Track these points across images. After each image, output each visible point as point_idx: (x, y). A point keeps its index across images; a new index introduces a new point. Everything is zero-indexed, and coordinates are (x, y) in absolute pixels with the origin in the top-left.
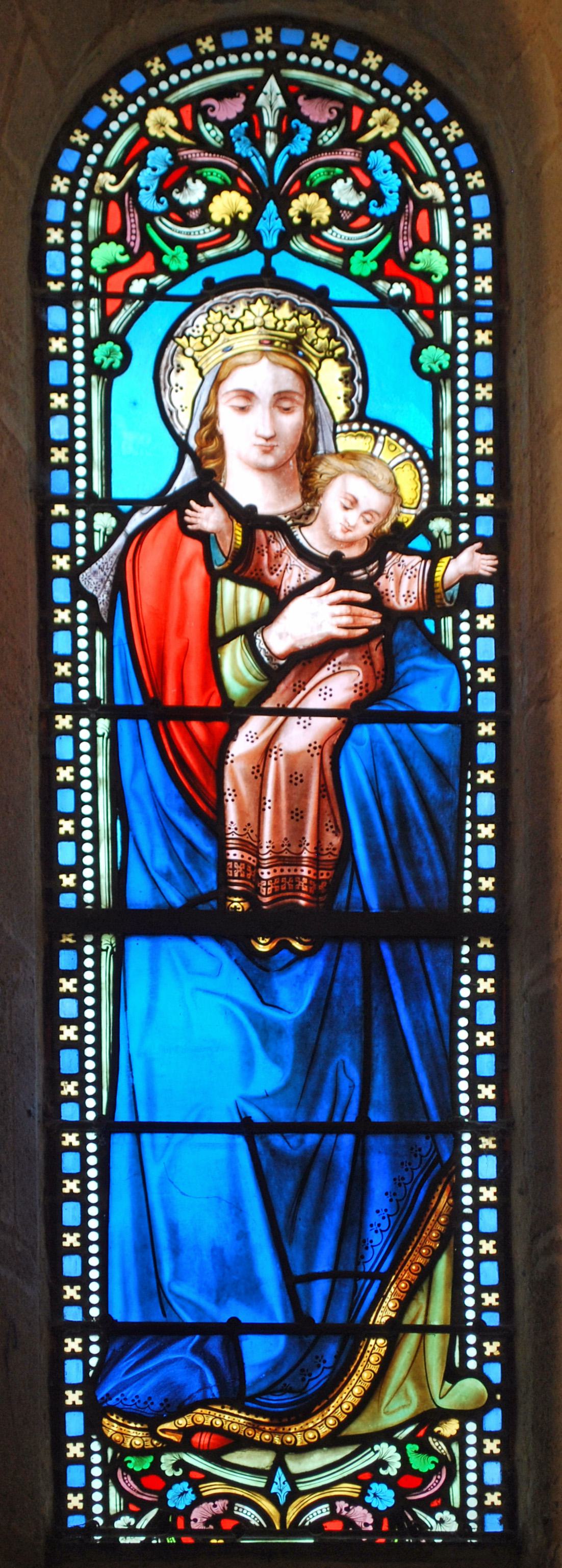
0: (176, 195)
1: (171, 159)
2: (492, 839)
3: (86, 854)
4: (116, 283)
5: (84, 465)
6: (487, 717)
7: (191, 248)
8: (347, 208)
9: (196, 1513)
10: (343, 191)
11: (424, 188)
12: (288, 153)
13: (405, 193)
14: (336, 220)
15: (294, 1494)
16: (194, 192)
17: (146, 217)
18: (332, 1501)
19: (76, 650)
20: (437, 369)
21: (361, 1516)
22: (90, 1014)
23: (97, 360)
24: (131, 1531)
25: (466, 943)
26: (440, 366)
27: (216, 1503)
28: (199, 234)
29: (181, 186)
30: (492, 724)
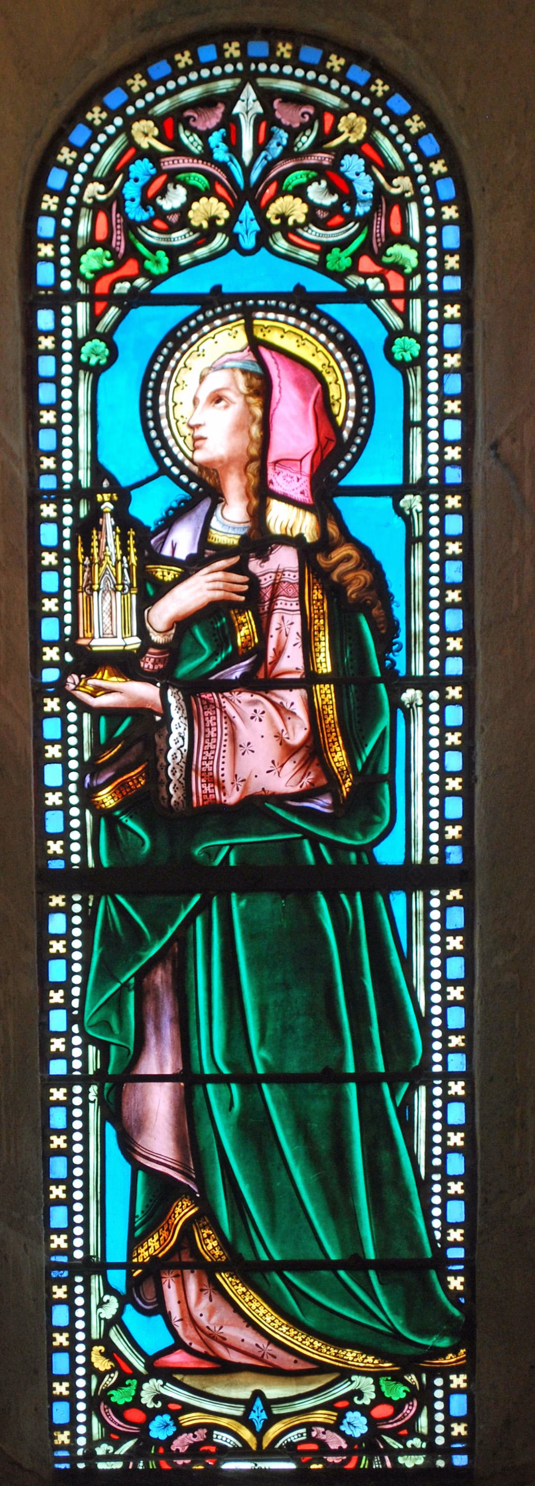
0: (159, 201)
2: (459, 460)
3: (80, 1178)
4: (102, 287)
7: (173, 253)
9: (177, 1445)
10: (317, 193)
11: (395, 182)
13: (378, 190)
15: (272, 1420)
16: (175, 198)
17: (131, 226)
18: (309, 1426)
19: (60, 399)
20: (408, 358)
21: (335, 1442)
22: (77, 1125)
24: (108, 1457)
27: (196, 1433)
30: (459, 689)
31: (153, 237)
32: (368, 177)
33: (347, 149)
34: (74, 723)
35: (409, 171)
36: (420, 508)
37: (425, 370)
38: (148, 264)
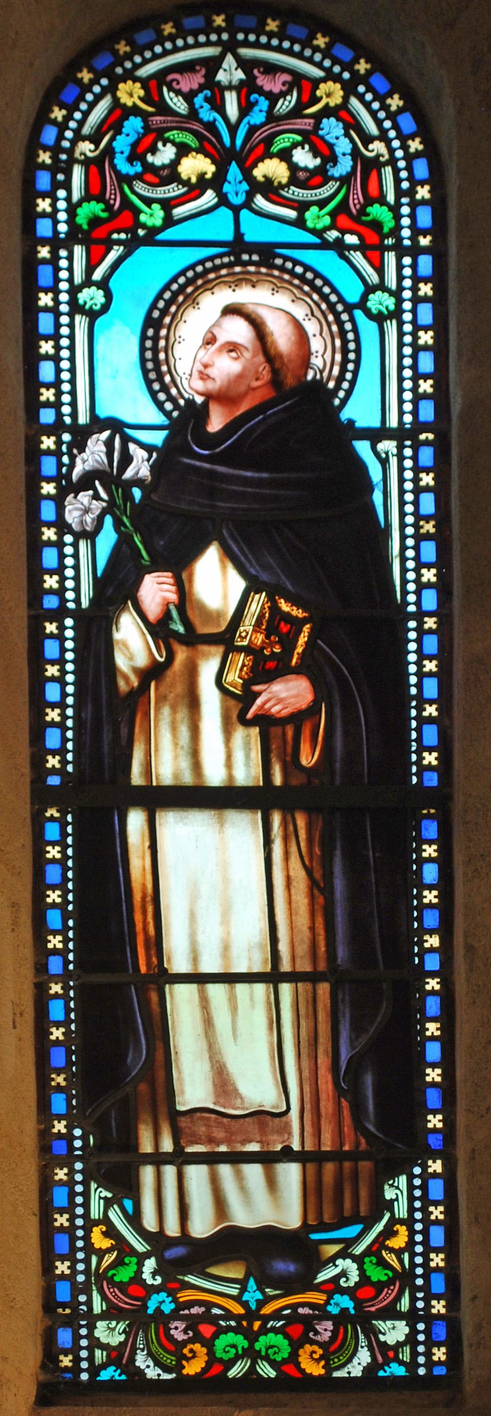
0: (150, 158)
1: (143, 128)
5: (68, 348)
6: (433, 974)
7: (168, 205)
8: (306, 169)
10: (304, 158)
11: (371, 147)
12: (249, 123)
13: (355, 154)
14: (294, 181)
16: (165, 155)
17: (128, 180)
20: (386, 312)
23: (81, 302)
25: (420, 1310)
26: (387, 308)
28: (169, 192)
29: (154, 150)
31: (140, 187)
32: (347, 140)
33: (327, 112)
34: (71, 545)
35: (383, 137)
36: (395, 451)
37: (401, 324)
38: (143, 218)
